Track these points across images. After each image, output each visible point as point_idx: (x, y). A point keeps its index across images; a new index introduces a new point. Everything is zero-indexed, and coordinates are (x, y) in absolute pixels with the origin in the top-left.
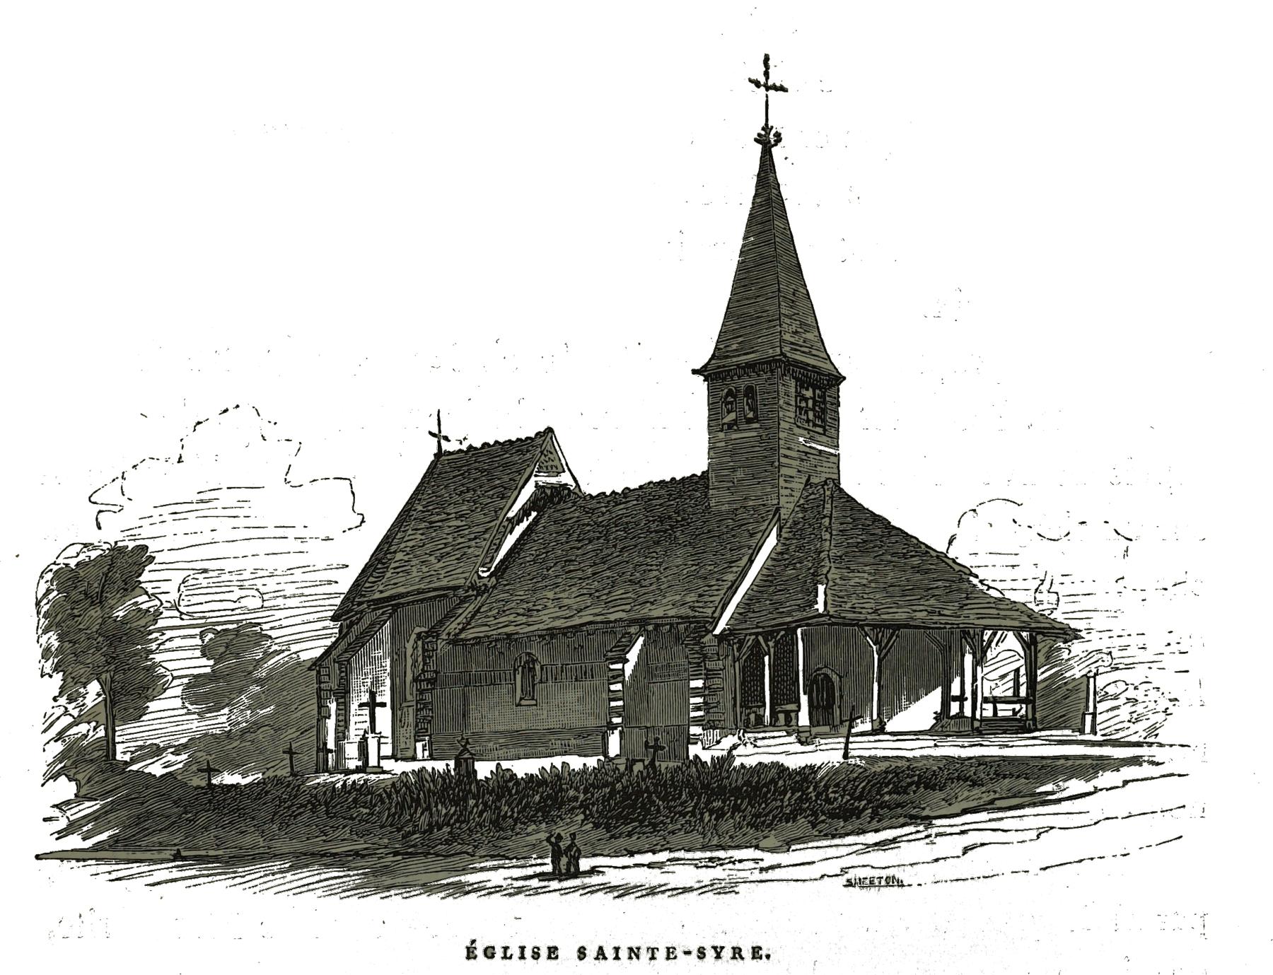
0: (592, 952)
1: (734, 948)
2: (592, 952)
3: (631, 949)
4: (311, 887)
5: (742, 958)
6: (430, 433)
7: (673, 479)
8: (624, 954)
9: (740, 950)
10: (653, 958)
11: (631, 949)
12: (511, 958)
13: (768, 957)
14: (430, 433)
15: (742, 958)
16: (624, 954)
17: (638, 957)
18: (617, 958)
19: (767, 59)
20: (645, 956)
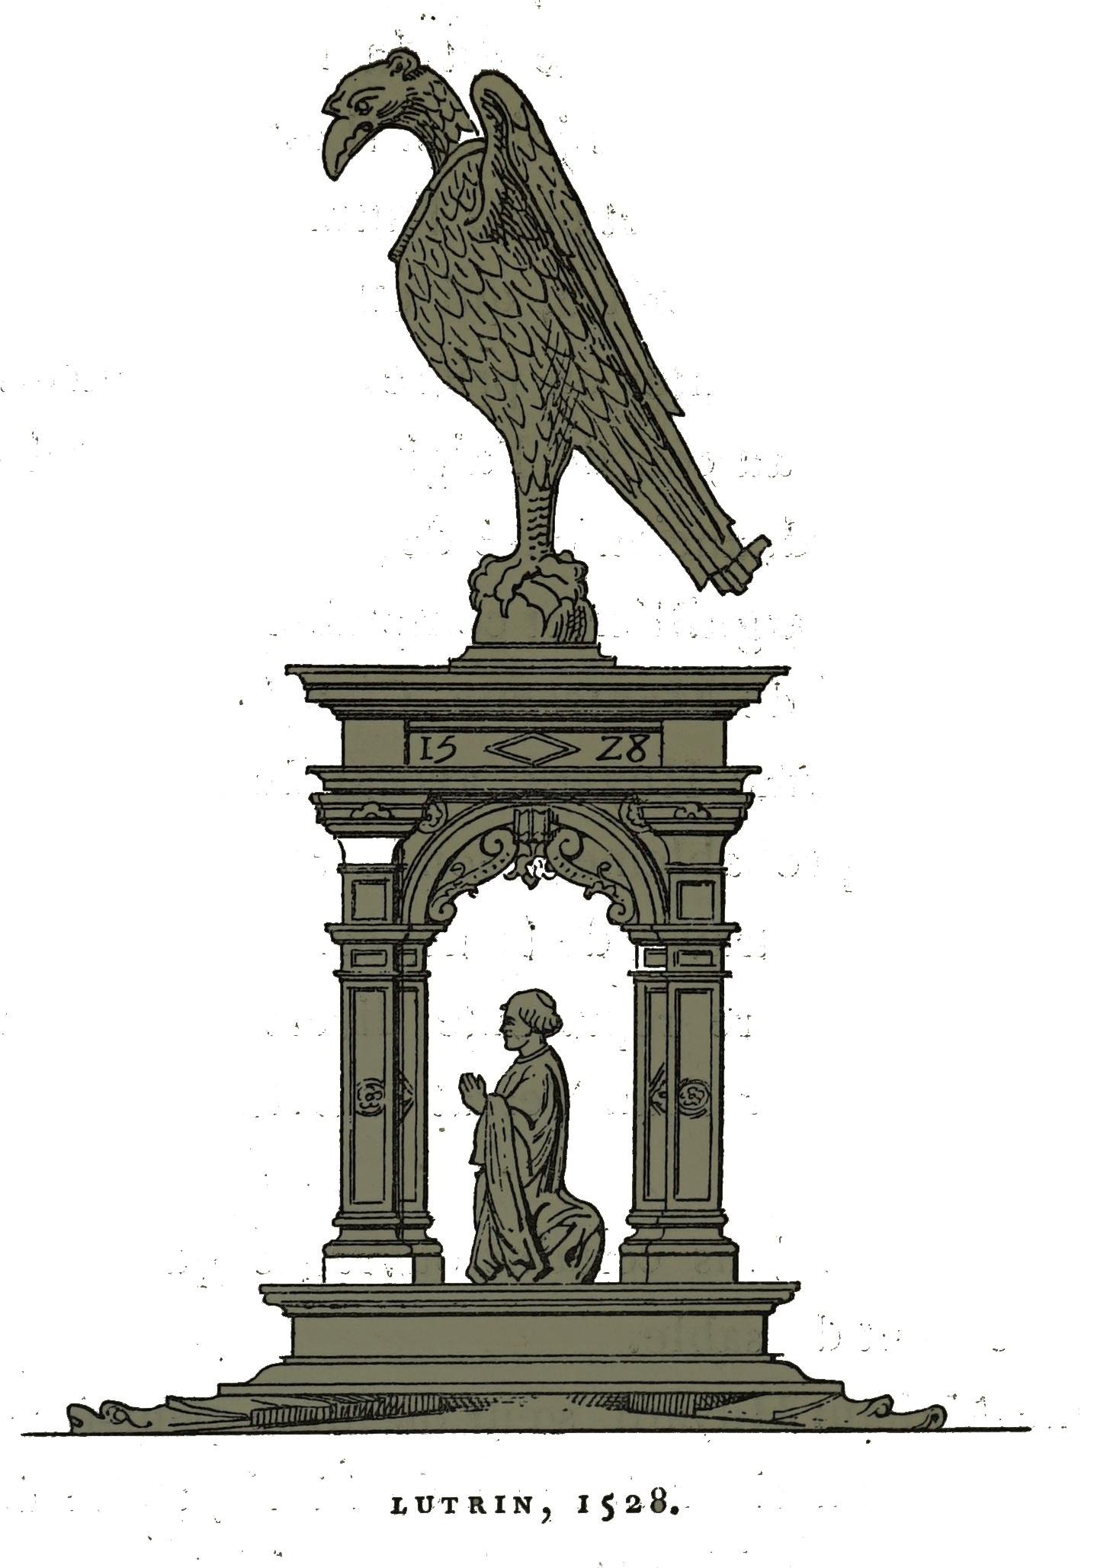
0: (462, 1506)
1: (472, 1499)
2: (462, 1506)
3: (518, 1499)
4: (701, 1249)
5: (482, 1511)
6: (758, 770)
7: (473, 892)
8: (509, 1504)
9: (480, 1500)
10: (450, 1511)
11: (518, 1499)
12: (405, 1511)
13: (675, 1510)
14: (758, 770)
15: (482, 1511)
16: (509, 1504)
17: (528, 1511)
18: (500, 1510)
19: (1028, 1429)
20: (440, 1508)
